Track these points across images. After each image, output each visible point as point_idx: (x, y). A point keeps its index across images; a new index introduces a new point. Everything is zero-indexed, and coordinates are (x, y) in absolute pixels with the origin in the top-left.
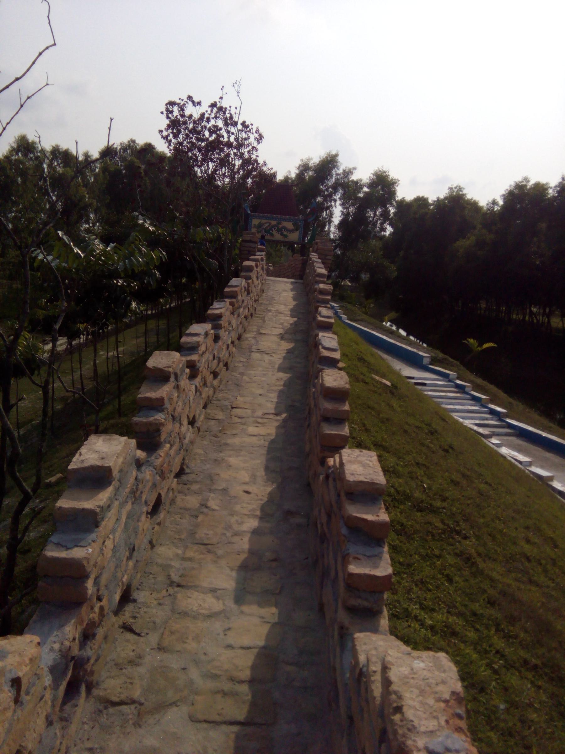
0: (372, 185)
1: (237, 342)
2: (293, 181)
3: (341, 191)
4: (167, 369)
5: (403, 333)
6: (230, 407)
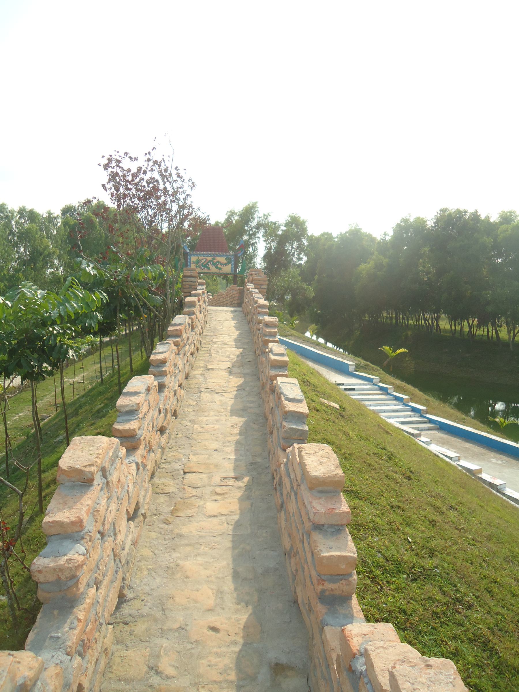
0: (288, 224)
1: (184, 382)
2: (222, 225)
4: (87, 469)
5: (321, 340)
6: (182, 473)
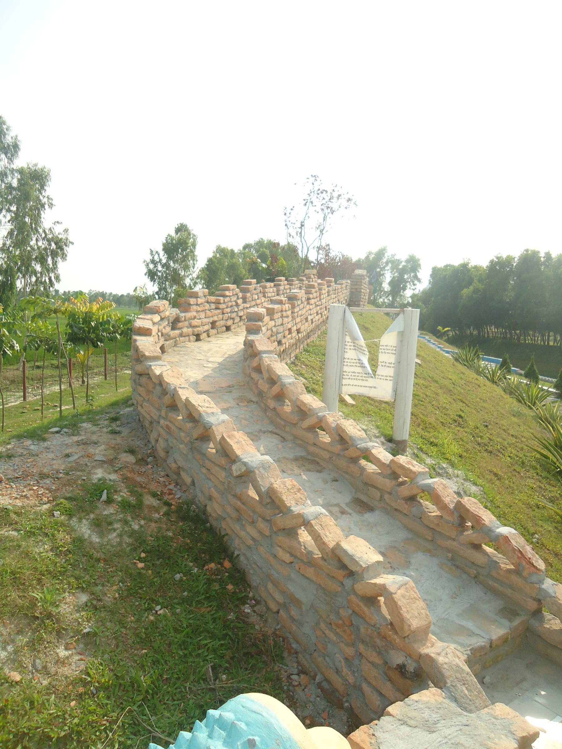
0: (407, 261)
2: (363, 260)
3: (390, 265)
